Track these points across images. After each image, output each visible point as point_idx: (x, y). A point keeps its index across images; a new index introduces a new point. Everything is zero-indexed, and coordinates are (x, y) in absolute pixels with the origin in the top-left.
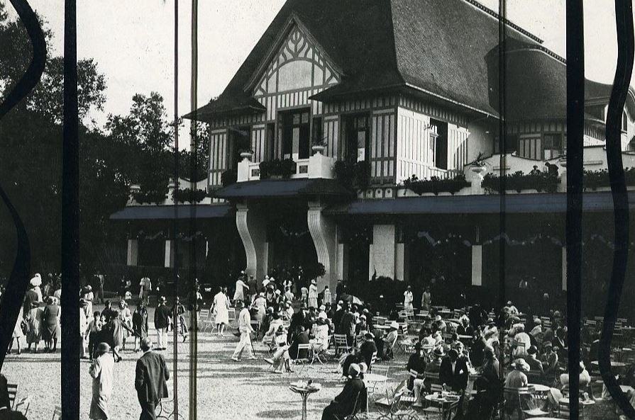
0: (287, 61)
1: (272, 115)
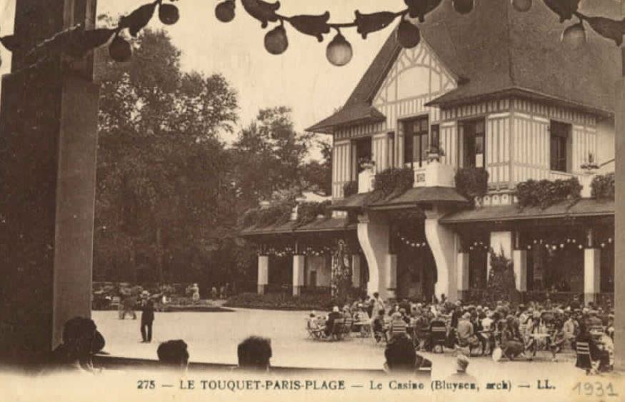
0: (405, 69)
1: (391, 124)
